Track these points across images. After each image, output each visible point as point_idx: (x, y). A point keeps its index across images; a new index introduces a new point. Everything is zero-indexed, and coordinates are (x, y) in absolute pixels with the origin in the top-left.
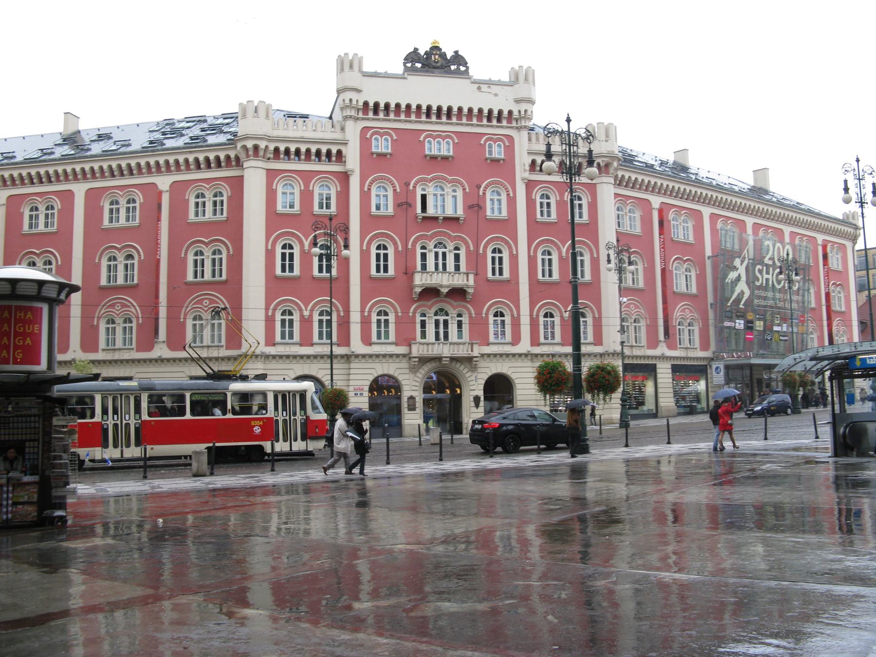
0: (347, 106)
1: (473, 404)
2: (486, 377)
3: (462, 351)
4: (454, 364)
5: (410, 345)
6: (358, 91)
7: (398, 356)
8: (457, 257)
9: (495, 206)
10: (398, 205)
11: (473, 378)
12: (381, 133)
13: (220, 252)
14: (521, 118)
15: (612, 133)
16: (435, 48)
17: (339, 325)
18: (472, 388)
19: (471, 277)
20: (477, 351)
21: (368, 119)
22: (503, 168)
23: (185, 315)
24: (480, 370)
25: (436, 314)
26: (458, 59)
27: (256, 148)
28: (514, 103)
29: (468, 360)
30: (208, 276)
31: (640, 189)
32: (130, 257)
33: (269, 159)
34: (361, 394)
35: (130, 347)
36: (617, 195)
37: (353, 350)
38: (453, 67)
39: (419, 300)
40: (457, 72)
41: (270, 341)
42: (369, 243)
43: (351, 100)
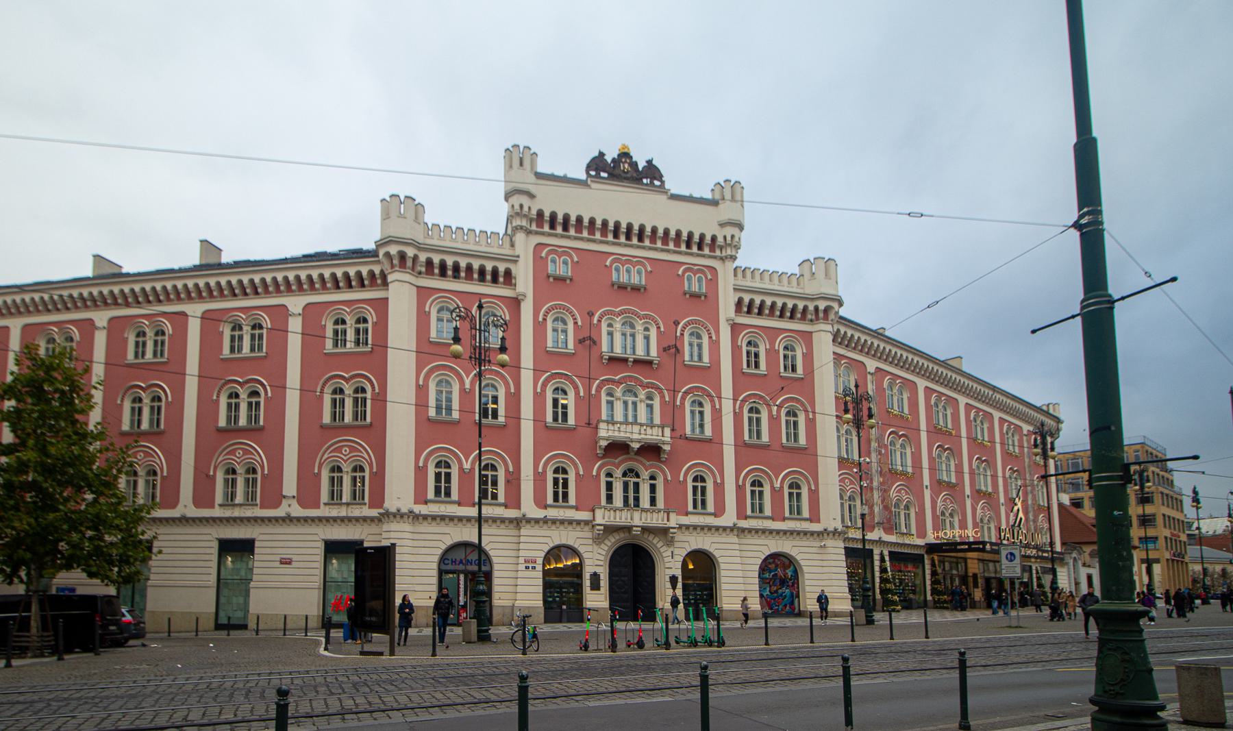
0: (517, 214)
1: (668, 585)
3: (656, 520)
7: (579, 522)
8: (653, 488)
13: (364, 390)
16: (625, 155)
17: (508, 482)
18: (667, 565)
19: (667, 431)
20: (675, 520)
22: (704, 301)
23: (215, 468)
24: (677, 545)
26: (652, 172)
27: (403, 256)
29: (663, 532)
30: (348, 418)
38: (645, 181)
39: (604, 457)
41: (421, 498)
42: (544, 385)
43: (521, 206)
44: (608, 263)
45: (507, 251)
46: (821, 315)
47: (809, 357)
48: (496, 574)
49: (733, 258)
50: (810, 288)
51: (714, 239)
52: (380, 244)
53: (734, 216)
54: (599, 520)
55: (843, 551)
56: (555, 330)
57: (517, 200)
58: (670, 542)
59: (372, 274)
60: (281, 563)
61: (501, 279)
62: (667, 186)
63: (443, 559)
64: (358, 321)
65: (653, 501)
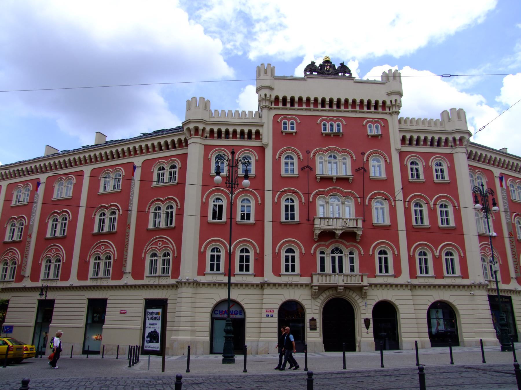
0: (263, 99)
1: (364, 325)
2: (374, 303)
3: (354, 282)
4: (347, 292)
5: (312, 277)
6: (271, 89)
7: (302, 285)
8: (352, 260)
9: (376, 169)
10: (302, 169)
11: (363, 303)
12: (286, 117)
13: (172, 207)
14: (392, 105)
15: (462, 116)
16: (327, 62)
17: (256, 260)
18: (363, 312)
19: (360, 222)
20: (366, 281)
21: (279, 109)
22: (380, 141)
24: (368, 297)
25: (332, 252)
26: (344, 68)
27: (197, 129)
28: (386, 96)
29: (359, 289)
31: (484, 162)
32: (114, 213)
33: (206, 137)
34: (272, 316)
35: (167, 275)
36: (469, 166)
37: (266, 279)
38: (340, 74)
40: (343, 78)
41: (201, 271)
42: (280, 197)
43: (266, 95)
44: (318, 122)
45: (257, 121)
46: (458, 143)
47: (452, 170)
48: (247, 320)
49: (398, 113)
50: (449, 127)
51: (384, 103)
52: (184, 124)
53: (395, 88)
54: (315, 282)
55: (487, 298)
56: (286, 164)
57: (263, 92)
58: (364, 296)
59: (180, 141)
60: (121, 313)
61: (253, 137)
62: (353, 76)
63: (214, 310)
64: (171, 168)
65: (352, 270)
